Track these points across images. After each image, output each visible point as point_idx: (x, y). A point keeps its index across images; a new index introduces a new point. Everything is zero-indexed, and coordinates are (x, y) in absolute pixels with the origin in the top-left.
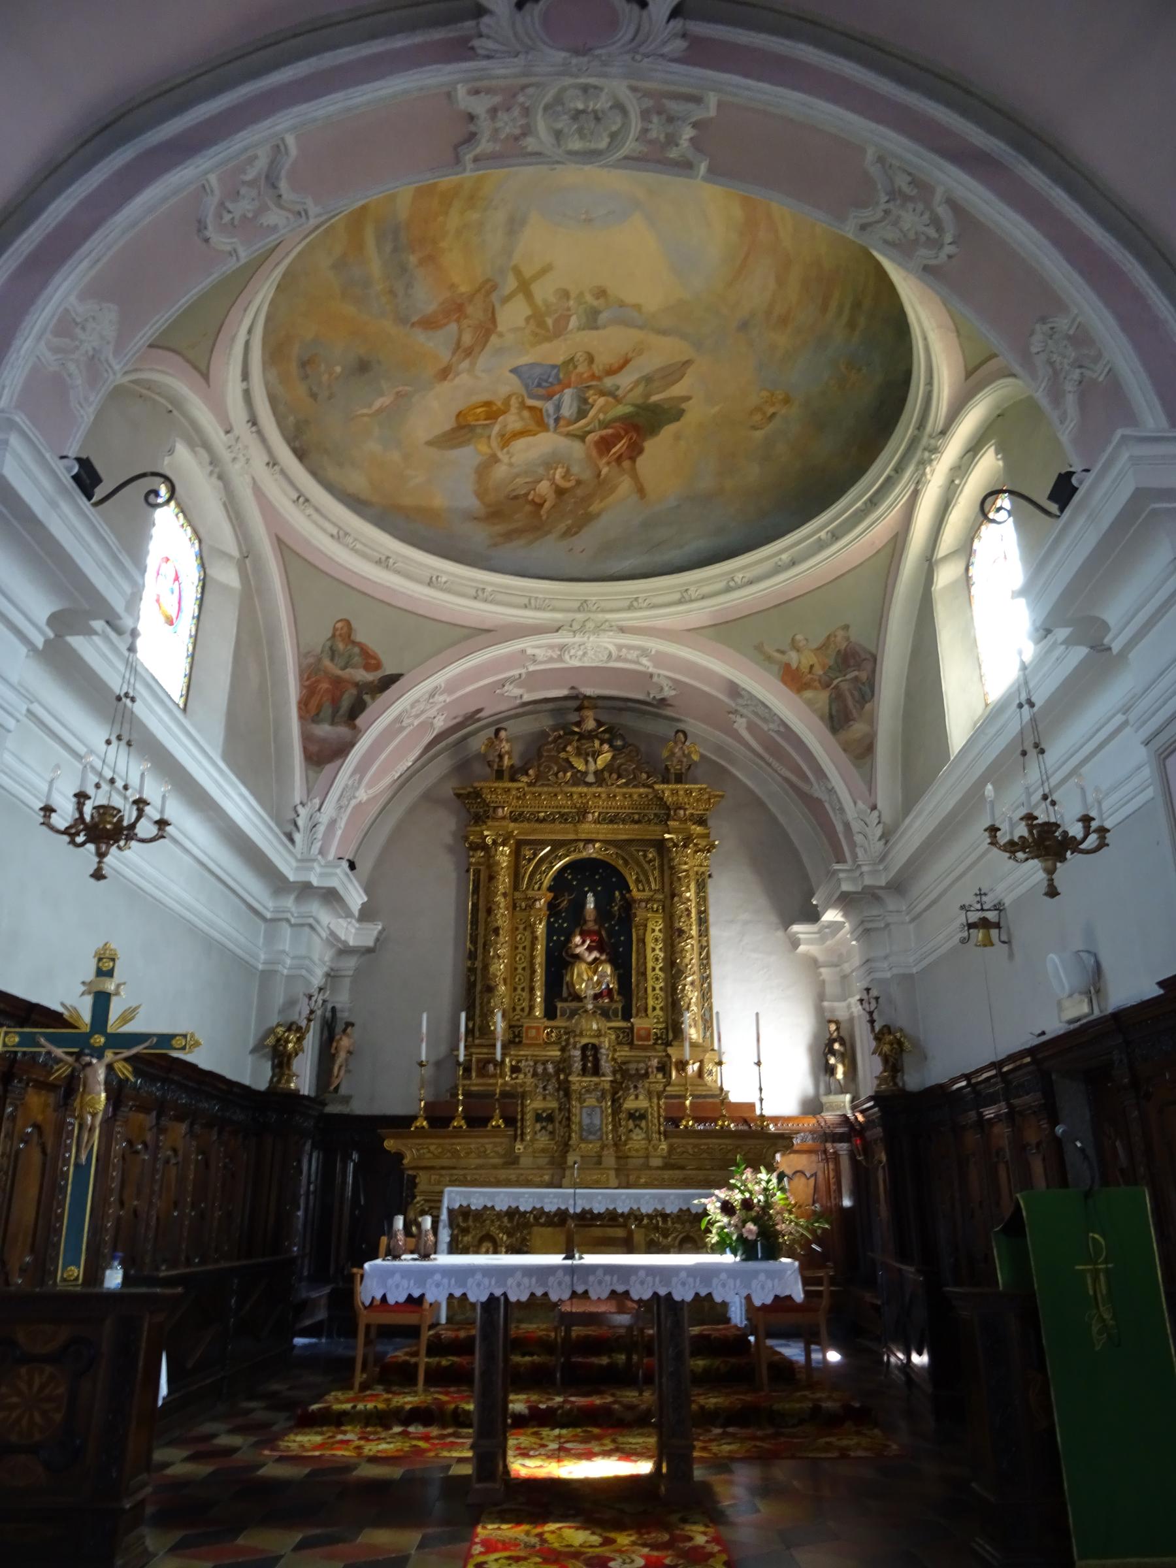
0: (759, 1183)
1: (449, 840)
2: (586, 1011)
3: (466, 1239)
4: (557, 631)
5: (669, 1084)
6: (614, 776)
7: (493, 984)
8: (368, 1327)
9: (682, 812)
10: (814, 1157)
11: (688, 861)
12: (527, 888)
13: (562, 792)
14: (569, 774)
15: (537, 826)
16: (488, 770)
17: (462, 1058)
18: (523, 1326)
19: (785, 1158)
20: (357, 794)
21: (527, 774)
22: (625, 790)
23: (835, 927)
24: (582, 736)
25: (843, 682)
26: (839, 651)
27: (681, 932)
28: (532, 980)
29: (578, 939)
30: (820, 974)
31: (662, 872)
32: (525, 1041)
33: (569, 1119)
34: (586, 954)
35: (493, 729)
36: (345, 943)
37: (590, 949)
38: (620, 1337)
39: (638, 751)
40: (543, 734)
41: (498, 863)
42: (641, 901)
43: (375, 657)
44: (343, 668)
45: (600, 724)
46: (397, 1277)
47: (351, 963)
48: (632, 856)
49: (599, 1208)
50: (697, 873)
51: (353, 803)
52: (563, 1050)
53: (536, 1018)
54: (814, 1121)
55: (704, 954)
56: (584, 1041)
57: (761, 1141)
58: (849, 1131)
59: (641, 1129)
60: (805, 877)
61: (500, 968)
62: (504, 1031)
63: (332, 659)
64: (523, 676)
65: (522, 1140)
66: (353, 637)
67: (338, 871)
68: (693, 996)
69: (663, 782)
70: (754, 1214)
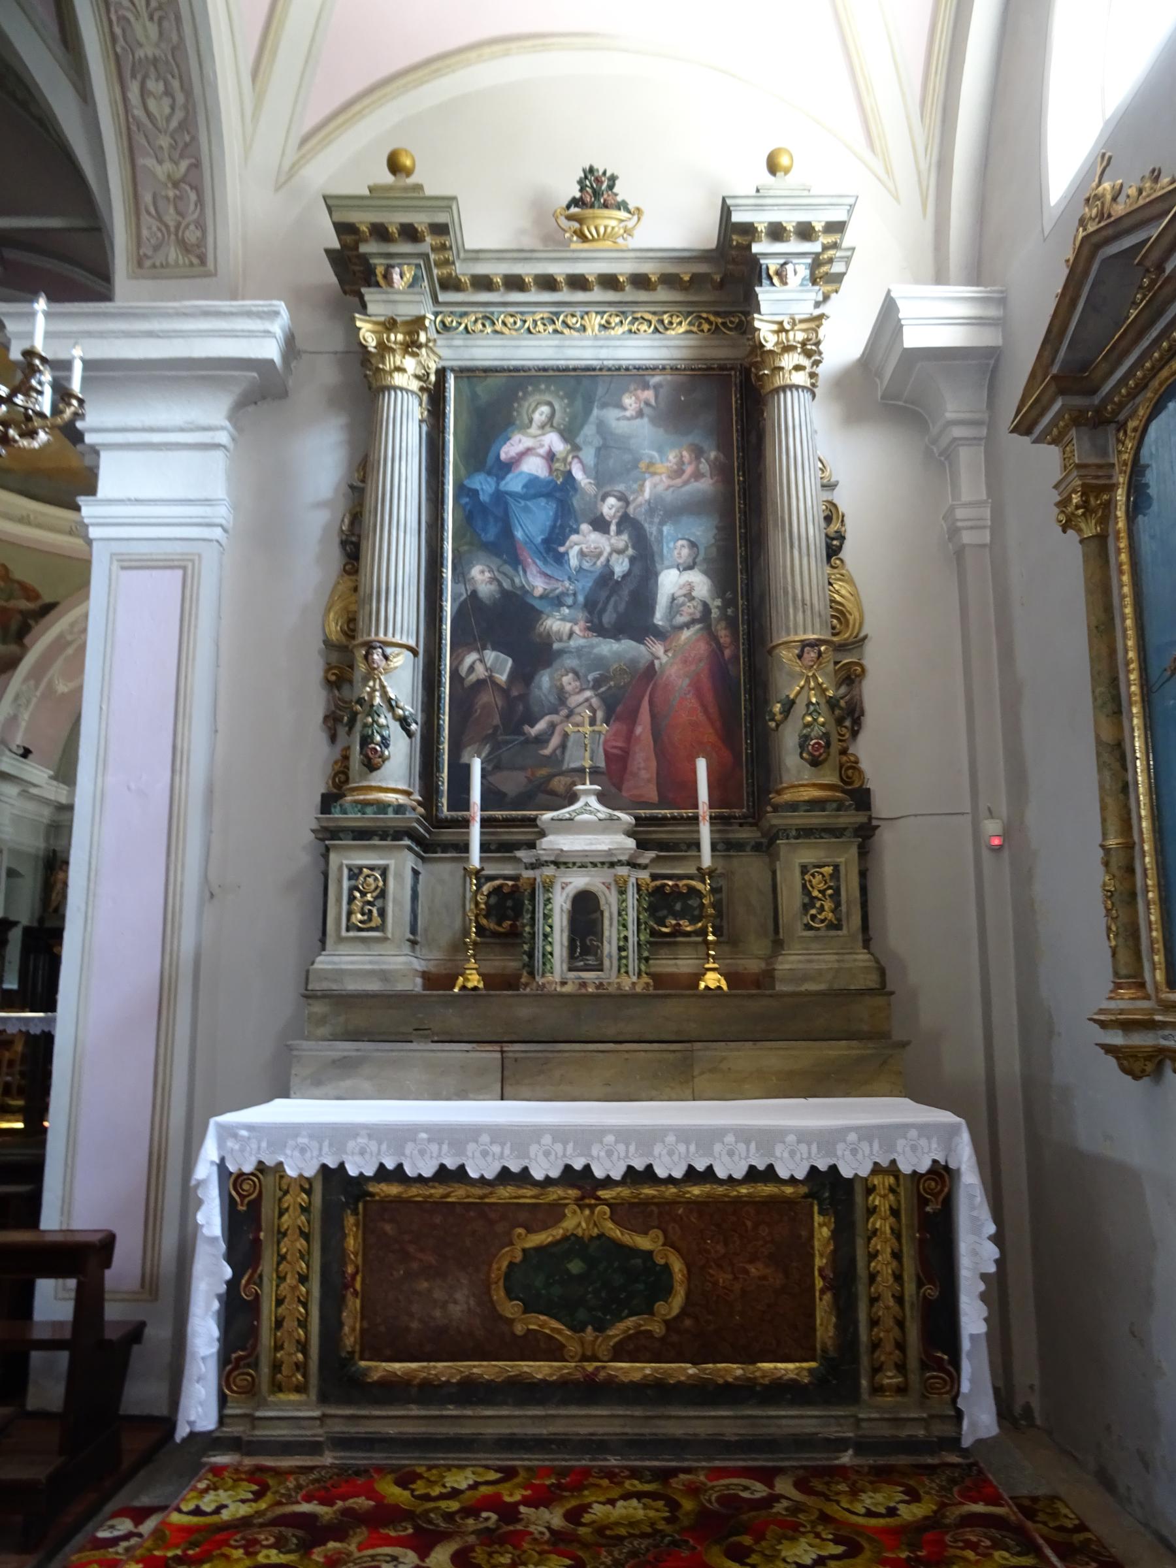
43: (34, 590)
44: (7, 600)
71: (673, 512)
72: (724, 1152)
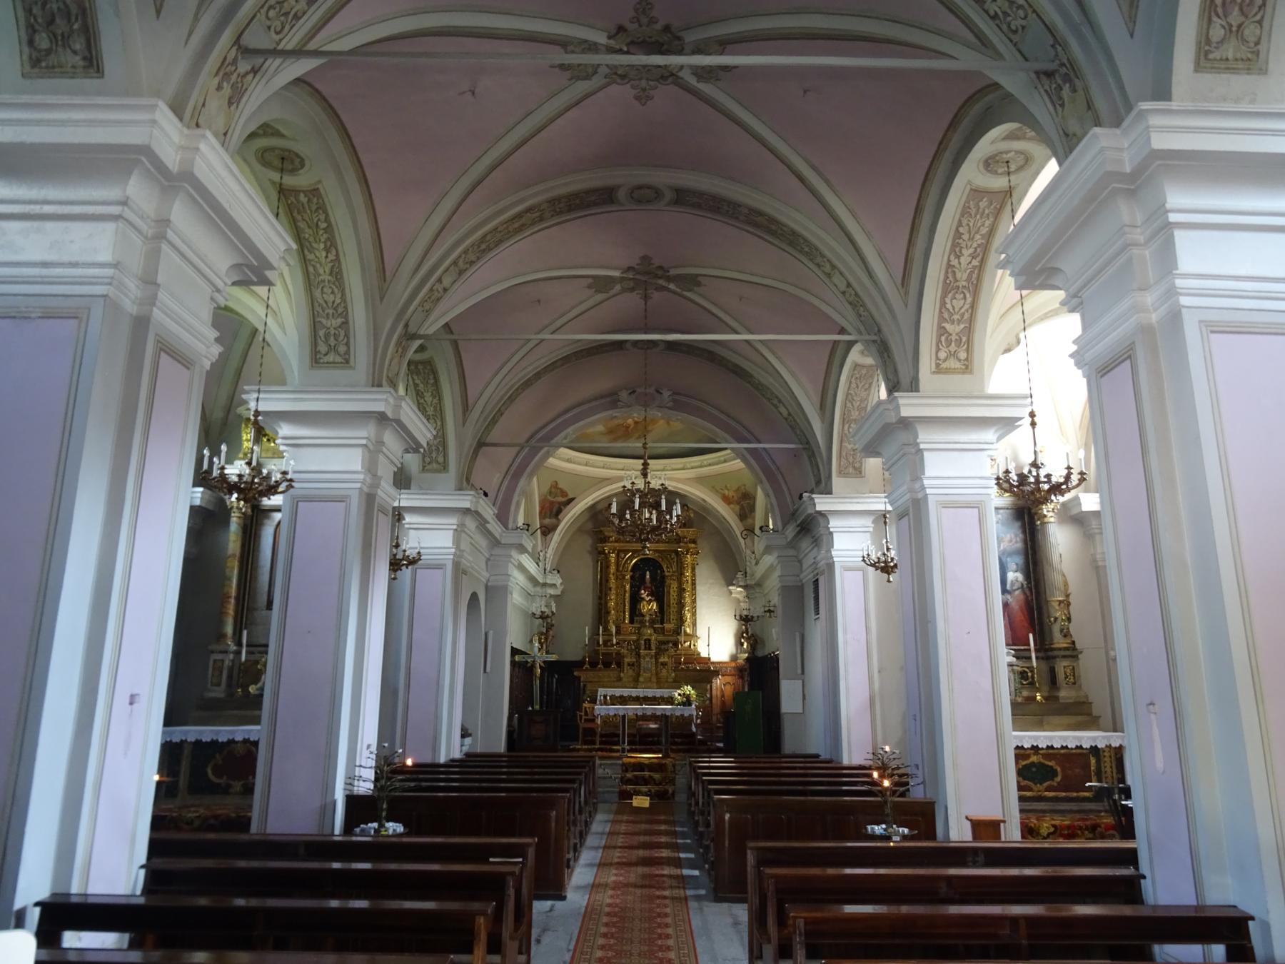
25: (745, 503)
49: (650, 695)
68: (688, 615)
71: (1010, 554)
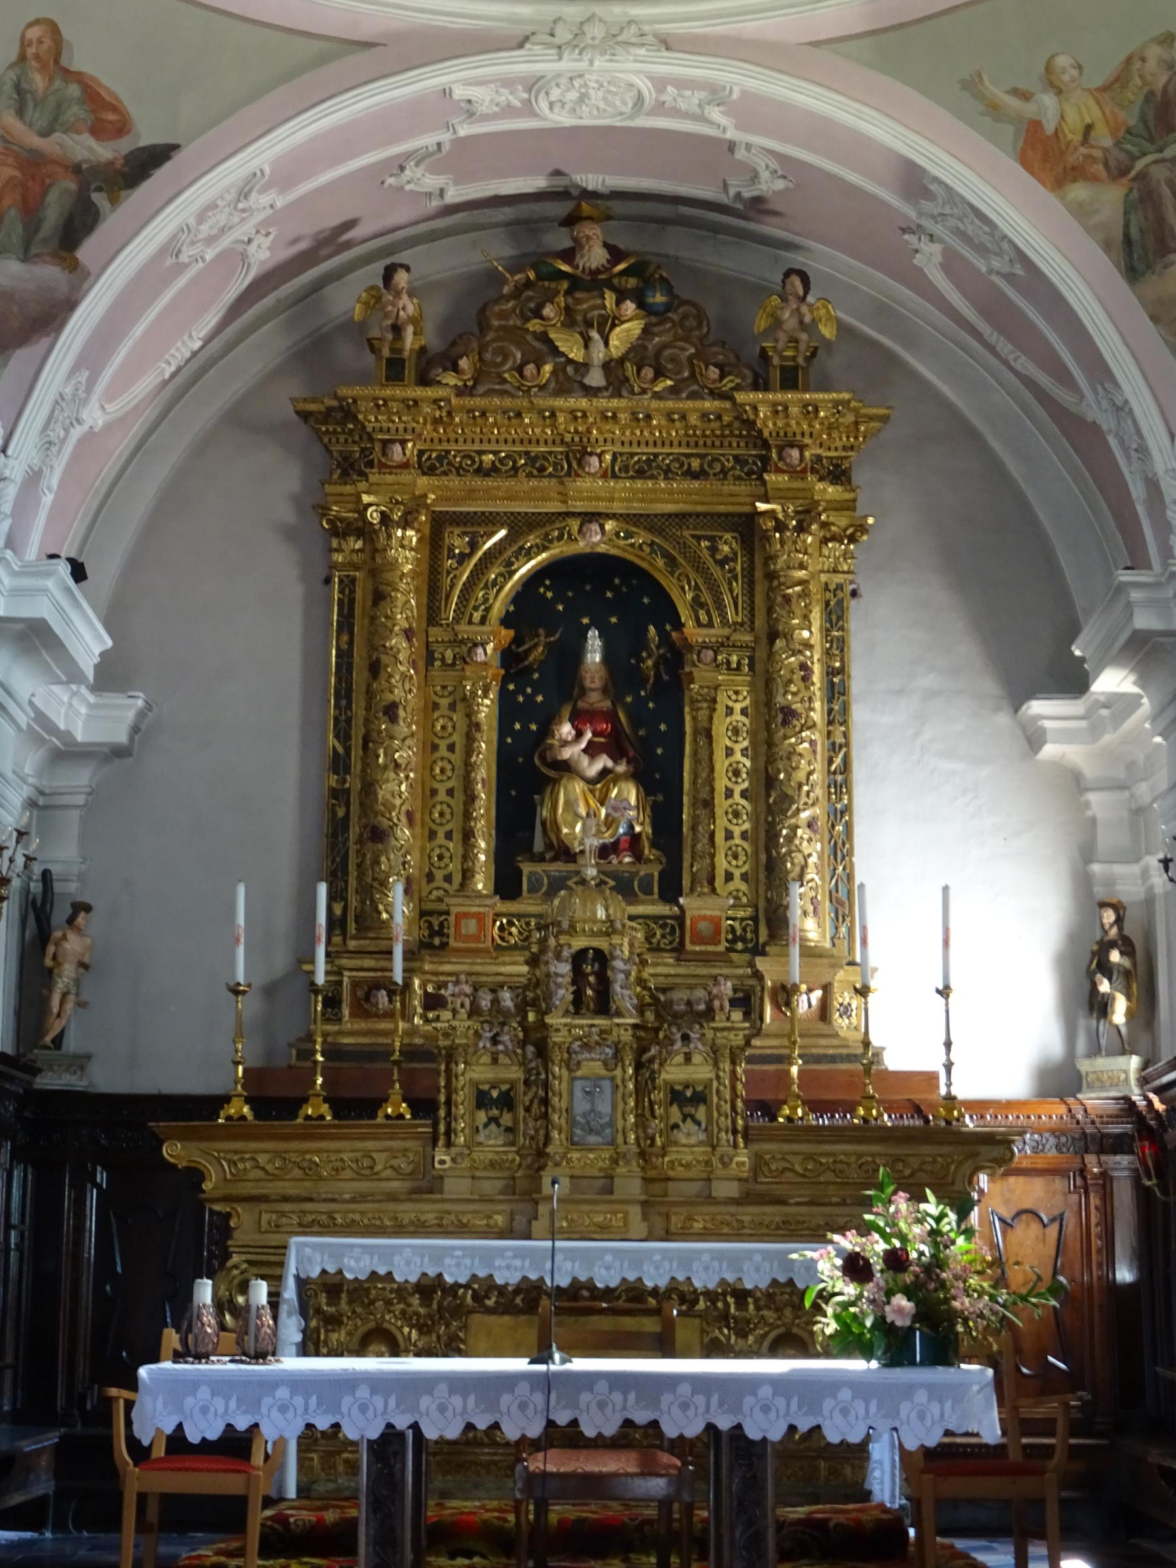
0: (920, 1221)
1: (286, 514)
2: (583, 882)
3: (334, 1336)
4: (521, 46)
5: (758, 1032)
6: (648, 372)
7: (386, 823)
8: (142, 1498)
9: (795, 453)
10: (1059, 1184)
11: (808, 562)
12: (457, 620)
13: (532, 407)
14: (548, 368)
15: (478, 482)
16: (370, 358)
17: (320, 979)
18: (454, 1503)
19: (999, 1186)
20: (84, 415)
21: (456, 369)
22: (670, 404)
23: (1121, 705)
24: (576, 284)
26: (1151, 93)
27: (789, 714)
28: (467, 815)
29: (566, 730)
30: (1087, 805)
31: (750, 585)
32: (452, 943)
33: (545, 1102)
34: (585, 760)
35: (379, 267)
36: (66, 737)
37: (591, 751)
38: (648, 1522)
39: (701, 316)
40: (493, 278)
41: (394, 565)
42: (705, 646)
44: (45, 134)
45: (616, 255)
46: (204, 1393)
47: (79, 780)
48: (684, 547)
49: (606, 1278)
50: (826, 587)
51: (77, 432)
52: (533, 962)
53: (479, 895)
54: (1062, 1110)
55: (838, 761)
56: (579, 943)
57: (946, 1149)
58: (1138, 1130)
59: (699, 1124)
60: (1063, 598)
61: (398, 790)
62: (410, 922)
63: (20, 112)
64: (446, 148)
65: (449, 1144)
66: (64, 62)
67: (50, 584)
68: (811, 849)
69: (756, 387)
70: (908, 1278)
72: (594, 1404)
